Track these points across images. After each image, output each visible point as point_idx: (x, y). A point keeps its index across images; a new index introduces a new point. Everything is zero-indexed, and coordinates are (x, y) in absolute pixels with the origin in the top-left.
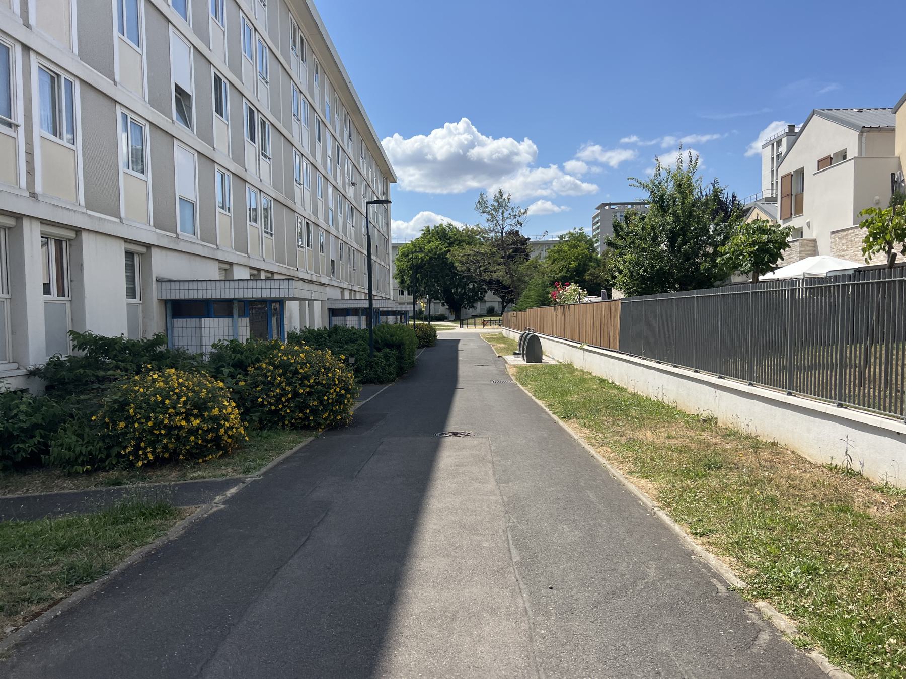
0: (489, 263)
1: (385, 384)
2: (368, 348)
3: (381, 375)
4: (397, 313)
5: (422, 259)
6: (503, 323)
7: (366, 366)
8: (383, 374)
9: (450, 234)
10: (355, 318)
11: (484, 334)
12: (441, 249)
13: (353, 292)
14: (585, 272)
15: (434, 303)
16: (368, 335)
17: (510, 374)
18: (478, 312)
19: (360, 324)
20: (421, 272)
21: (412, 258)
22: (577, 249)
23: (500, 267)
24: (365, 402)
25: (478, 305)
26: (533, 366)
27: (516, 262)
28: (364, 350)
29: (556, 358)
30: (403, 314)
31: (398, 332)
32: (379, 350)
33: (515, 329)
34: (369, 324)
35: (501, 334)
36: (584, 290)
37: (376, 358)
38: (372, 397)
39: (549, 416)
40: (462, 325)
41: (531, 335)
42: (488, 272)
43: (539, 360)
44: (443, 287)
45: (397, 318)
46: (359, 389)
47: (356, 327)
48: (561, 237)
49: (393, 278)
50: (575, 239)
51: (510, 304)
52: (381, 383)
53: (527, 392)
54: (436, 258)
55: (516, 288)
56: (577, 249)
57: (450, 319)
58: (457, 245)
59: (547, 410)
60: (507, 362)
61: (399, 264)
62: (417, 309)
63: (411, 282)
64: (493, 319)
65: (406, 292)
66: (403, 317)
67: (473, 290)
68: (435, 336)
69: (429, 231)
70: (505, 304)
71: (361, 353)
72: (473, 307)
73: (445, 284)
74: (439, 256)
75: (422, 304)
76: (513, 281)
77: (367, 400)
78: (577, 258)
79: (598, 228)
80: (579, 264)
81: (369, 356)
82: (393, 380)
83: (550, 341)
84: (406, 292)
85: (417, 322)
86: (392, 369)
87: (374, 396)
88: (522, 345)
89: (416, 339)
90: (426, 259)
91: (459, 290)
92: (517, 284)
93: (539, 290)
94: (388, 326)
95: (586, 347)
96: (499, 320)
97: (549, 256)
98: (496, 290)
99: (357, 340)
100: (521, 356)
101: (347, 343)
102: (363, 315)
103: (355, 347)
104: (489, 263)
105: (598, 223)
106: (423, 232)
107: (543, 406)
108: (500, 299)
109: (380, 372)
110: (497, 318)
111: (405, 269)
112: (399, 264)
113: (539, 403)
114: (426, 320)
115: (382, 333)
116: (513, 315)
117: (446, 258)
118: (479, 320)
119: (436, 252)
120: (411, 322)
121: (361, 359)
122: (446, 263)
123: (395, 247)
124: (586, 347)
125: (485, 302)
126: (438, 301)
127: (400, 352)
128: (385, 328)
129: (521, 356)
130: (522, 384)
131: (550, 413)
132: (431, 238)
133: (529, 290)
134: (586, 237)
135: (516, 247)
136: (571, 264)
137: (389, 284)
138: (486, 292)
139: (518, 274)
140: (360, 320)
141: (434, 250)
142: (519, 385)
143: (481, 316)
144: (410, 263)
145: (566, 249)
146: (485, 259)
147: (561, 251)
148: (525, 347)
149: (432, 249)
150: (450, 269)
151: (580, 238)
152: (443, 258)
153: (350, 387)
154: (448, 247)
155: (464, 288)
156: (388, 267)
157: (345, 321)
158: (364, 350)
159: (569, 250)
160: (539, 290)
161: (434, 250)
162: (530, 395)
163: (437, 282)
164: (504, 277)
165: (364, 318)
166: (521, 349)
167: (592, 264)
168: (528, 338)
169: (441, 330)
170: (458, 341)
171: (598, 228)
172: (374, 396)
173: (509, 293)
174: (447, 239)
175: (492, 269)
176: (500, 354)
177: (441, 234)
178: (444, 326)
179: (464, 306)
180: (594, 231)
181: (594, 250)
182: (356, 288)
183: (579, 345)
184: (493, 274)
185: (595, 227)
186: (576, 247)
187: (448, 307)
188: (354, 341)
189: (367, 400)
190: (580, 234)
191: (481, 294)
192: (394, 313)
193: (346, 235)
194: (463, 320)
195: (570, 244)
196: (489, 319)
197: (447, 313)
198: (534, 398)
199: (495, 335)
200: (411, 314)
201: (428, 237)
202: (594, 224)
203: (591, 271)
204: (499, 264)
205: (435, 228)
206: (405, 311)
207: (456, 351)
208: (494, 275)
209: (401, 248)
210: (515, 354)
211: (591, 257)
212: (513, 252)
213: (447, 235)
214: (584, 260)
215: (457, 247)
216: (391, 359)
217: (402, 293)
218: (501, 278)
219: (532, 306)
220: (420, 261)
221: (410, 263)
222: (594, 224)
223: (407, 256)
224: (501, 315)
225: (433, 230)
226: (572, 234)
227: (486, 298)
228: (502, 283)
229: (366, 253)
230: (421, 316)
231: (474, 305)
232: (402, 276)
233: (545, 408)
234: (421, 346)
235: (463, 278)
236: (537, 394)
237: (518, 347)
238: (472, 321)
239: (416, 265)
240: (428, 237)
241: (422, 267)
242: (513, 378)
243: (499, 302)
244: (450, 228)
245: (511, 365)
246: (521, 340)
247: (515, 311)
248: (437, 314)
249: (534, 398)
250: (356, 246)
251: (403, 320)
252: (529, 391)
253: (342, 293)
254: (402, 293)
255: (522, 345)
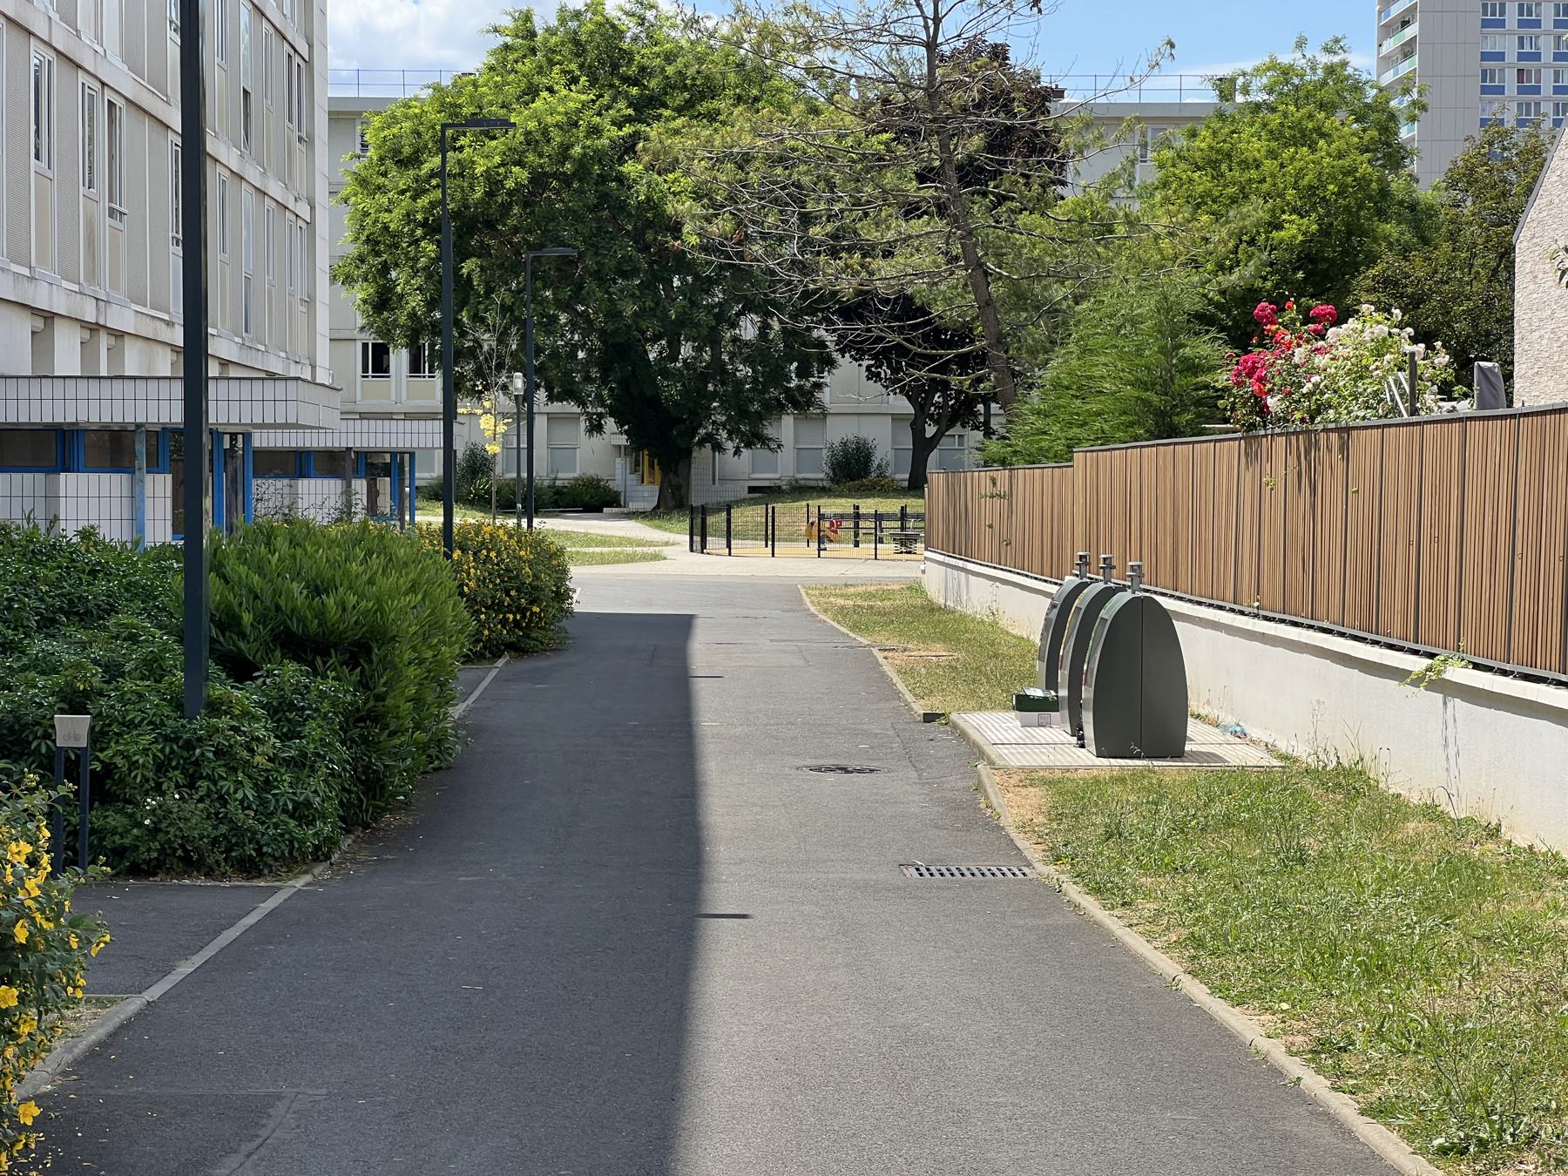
0: (857, 203)
1: (278, 877)
2: (175, 655)
3: (247, 820)
4: (348, 466)
5: (493, 182)
6: (928, 530)
7: (161, 767)
8: (264, 814)
9: (645, 55)
10: (114, 483)
11: (824, 589)
12: (595, 131)
13: (104, 341)
14: (1355, 269)
15: (551, 417)
16: (178, 582)
17: (1009, 820)
18: (782, 466)
19: (137, 521)
20: (483, 251)
21: (440, 173)
22: (1313, 148)
23: (917, 226)
24: (134, 1004)
25: (785, 428)
26: (1137, 775)
27: (1002, 199)
28: (153, 668)
29: (1254, 733)
30: (386, 470)
31: (354, 567)
32: (241, 670)
33: (999, 563)
34: (187, 518)
35: (916, 588)
36: (1430, 347)
37: (223, 722)
38: (185, 969)
39: (1346, 1133)
40: (699, 537)
41: (1125, 597)
42: (850, 250)
43: (1170, 745)
44: (603, 334)
45: (348, 492)
46: (86, 942)
47: (113, 532)
48: (1225, 87)
49: (334, 279)
50: (1301, 96)
51: (957, 430)
52: (249, 868)
53: (1135, 941)
54: (566, 180)
55: (1000, 341)
56: (1313, 148)
57: (633, 506)
58: (680, 111)
59: (1316, 1084)
60: (981, 754)
61: (369, 204)
62: (460, 447)
63: (431, 304)
64: (868, 505)
65: (399, 359)
66: (385, 484)
67: (757, 353)
68: (562, 595)
69: (532, 34)
70: (930, 430)
71: (128, 685)
72: (755, 438)
73: (614, 314)
74: (583, 165)
75: (486, 422)
76: (987, 304)
77: (154, 993)
78: (1311, 196)
79: (1407, 51)
80: (1325, 231)
81: (178, 705)
82: (320, 854)
83: (1222, 636)
84: (399, 359)
85: (465, 518)
86: (317, 790)
87: (198, 960)
88: (1066, 651)
89: (455, 613)
90: (510, 184)
91: (686, 350)
92: (1007, 319)
93: (1139, 352)
94: (300, 533)
95: (1459, 673)
96: (903, 516)
97: (1165, 185)
98: (881, 357)
99: (112, 610)
100: (1060, 717)
101: (47, 624)
102: (154, 467)
103: (97, 652)
104: (857, 203)
105: (1405, 24)
106: (500, 40)
107: (1276, 1050)
108: (903, 405)
109: (244, 804)
110: (892, 505)
111: (397, 235)
112: (369, 204)
113: (1246, 1024)
114: (507, 507)
115: (260, 571)
116: (987, 488)
117: (621, 179)
118: (792, 514)
119: (565, 148)
120: (430, 517)
121: (131, 725)
122: (621, 207)
123: (344, 117)
124: (1459, 673)
125: (824, 415)
126: (571, 407)
127: (364, 684)
128: (281, 544)
129: (1060, 717)
130: (1097, 891)
131: (1345, 1107)
132: (540, 70)
133: (1086, 351)
134: (1357, 88)
135: (1002, 119)
136: (1279, 227)
137: (310, 302)
138: (829, 363)
139: (1011, 268)
140: (136, 499)
141: (557, 137)
142: (1074, 892)
143: (800, 490)
144: (424, 201)
145: (1254, 146)
146: (838, 179)
147: (1229, 156)
148: (1092, 665)
149: (545, 132)
150: (637, 236)
151: (1324, 95)
152: (603, 179)
153: (21, 935)
154: (629, 120)
155: (713, 340)
156: (303, 210)
157: (52, 497)
158: (153, 668)
159: (1273, 154)
160: (1139, 352)
161: (557, 137)
162: (1168, 965)
163: (567, 307)
164: (934, 278)
165: (159, 488)
166: (1063, 675)
167: (1390, 228)
168: (1109, 611)
169: (592, 560)
170: (682, 625)
171: (1407, 51)
172: (198, 960)
173: (964, 363)
174: (626, 79)
175: (875, 235)
176: (935, 704)
177: (592, 55)
178: (604, 541)
179: (709, 438)
180: (1386, 62)
181: (1394, 156)
182: (122, 318)
183: (1417, 664)
184: (877, 263)
185: (1391, 45)
186: (1305, 137)
187: (623, 440)
188: (85, 614)
189: (154, 993)
190: (1330, 70)
191: (803, 373)
192: (332, 463)
193: (70, 20)
194: (704, 511)
195: (1275, 120)
196: (843, 505)
197: (618, 473)
198: (1197, 990)
199: (886, 595)
200: (430, 471)
201: (527, 66)
202: (1387, 30)
203: (1388, 263)
204: (912, 211)
205: (563, 21)
206: (387, 370)
207: (679, 684)
208: (885, 269)
209: (377, 121)
210: (1024, 704)
211: (1384, 193)
212: (990, 148)
213: (629, 56)
214: (1347, 209)
215: (679, 122)
216: (313, 729)
217: (378, 362)
218: (921, 284)
219: (1105, 439)
220: (479, 193)
221: (424, 201)
222: (1387, 30)
223: (413, 161)
224: (917, 484)
225: (551, 32)
226: (1286, 72)
227: (825, 396)
228: (923, 311)
229: (175, 119)
230: (480, 483)
231: (770, 431)
232: (385, 269)
233: (1295, 1068)
234: (485, 651)
235: (706, 285)
236: (1208, 961)
237: (1040, 667)
238: (749, 516)
239: (456, 215)
240: (527, 66)
241: (490, 225)
242: (1032, 850)
243: (896, 418)
244: (642, 21)
245: (1008, 771)
246: (1056, 628)
247: (1003, 463)
248: (566, 477)
249: (1197, 990)
250: (126, 83)
251: (385, 503)
252: (1150, 937)
253: (42, 340)
254: (378, 362)
255: (1066, 651)
